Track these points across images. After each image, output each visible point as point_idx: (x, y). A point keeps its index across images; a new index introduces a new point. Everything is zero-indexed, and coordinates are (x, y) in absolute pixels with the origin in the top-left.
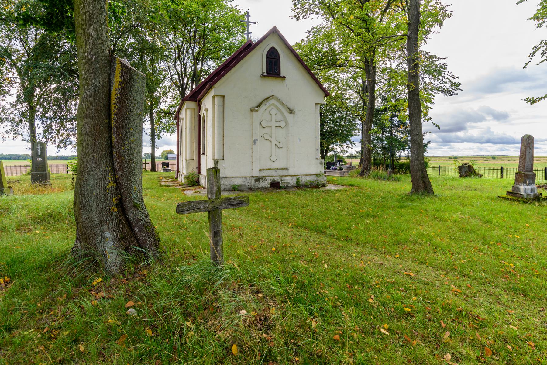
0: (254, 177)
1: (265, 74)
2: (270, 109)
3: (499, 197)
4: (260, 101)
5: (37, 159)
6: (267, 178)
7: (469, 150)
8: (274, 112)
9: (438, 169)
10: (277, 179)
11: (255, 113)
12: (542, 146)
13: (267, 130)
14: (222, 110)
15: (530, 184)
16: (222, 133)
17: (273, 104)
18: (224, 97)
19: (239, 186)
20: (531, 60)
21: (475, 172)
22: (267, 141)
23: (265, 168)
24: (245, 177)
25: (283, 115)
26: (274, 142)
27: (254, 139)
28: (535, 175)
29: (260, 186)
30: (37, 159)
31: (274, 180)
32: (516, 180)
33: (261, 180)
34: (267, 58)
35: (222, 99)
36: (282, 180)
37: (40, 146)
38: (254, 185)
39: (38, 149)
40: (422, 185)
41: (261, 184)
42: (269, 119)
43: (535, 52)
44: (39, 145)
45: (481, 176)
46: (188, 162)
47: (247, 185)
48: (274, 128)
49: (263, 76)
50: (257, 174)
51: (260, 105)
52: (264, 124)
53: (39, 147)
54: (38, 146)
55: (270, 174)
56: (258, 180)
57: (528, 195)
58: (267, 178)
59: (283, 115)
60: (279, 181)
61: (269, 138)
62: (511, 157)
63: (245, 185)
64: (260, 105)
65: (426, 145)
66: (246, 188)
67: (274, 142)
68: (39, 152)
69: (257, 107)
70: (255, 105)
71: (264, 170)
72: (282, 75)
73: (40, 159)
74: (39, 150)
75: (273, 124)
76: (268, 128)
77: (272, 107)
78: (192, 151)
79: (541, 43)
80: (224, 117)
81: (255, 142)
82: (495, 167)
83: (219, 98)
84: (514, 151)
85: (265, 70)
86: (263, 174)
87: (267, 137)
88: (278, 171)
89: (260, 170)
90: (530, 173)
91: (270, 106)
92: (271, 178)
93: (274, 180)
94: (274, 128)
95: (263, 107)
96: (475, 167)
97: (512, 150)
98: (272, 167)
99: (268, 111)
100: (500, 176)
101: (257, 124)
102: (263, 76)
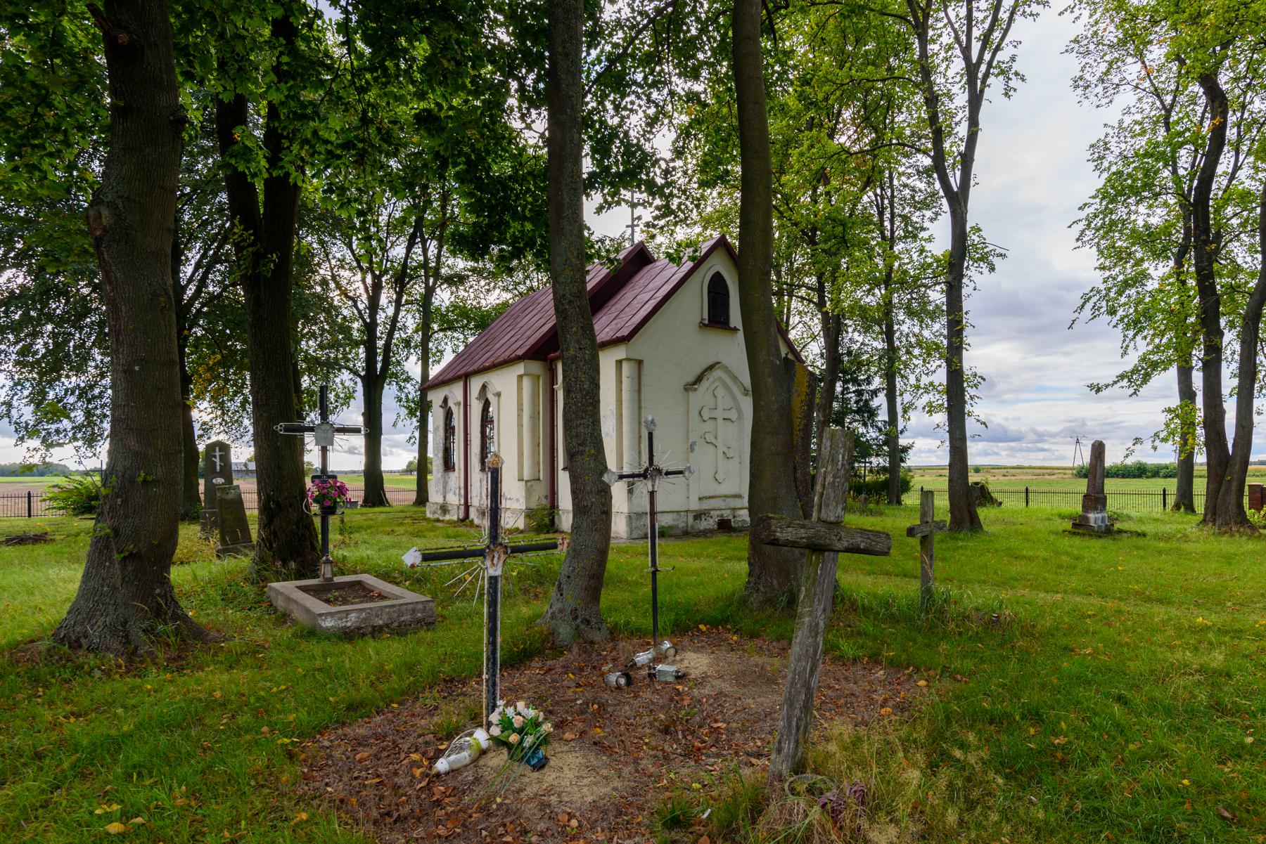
0: (692, 511)
1: (706, 322)
2: (714, 386)
3: (1065, 531)
4: (699, 371)
5: (214, 481)
6: (712, 513)
7: (928, 455)
8: (720, 392)
9: (1024, 495)
10: (727, 514)
11: (692, 395)
12: (1053, 447)
13: (709, 426)
14: (636, 388)
15: (1101, 511)
16: (637, 430)
17: (720, 379)
18: (640, 363)
19: (671, 527)
20: (1080, 316)
21: (991, 498)
22: (710, 446)
23: (707, 494)
24: (677, 512)
25: (734, 398)
26: (721, 448)
27: (691, 441)
28: (1105, 498)
29: (702, 528)
30: (214, 481)
31: (722, 516)
32: (1084, 507)
33: (703, 517)
34: (709, 292)
35: (636, 367)
36: (734, 517)
37: (220, 451)
38: (692, 527)
39: (215, 457)
40: (968, 519)
41: (704, 524)
42: (713, 406)
43: (1085, 303)
44: (217, 449)
45: (1001, 503)
46: (529, 484)
47: (681, 526)
48: (720, 421)
49: (703, 326)
50: (695, 505)
51: (699, 380)
52: (706, 415)
53: (218, 454)
54: (215, 451)
55: (716, 506)
56: (698, 516)
57: (1100, 527)
58: (712, 513)
59: (734, 398)
60: (731, 517)
61: (714, 441)
62: (1005, 468)
63: (677, 527)
64: (699, 380)
65: (905, 449)
66: (679, 532)
67: (721, 448)
68: (218, 463)
69: (695, 383)
70: (691, 379)
71: (707, 498)
72: (732, 325)
73: (220, 480)
74: (217, 460)
75: (720, 414)
76: (711, 423)
77: (717, 383)
78: (536, 464)
79: (1092, 291)
80: (640, 401)
81: (692, 448)
82: (1017, 489)
83: (632, 363)
84: (1008, 456)
85: (706, 316)
86: (706, 505)
87: (710, 438)
88: (728, 500)
89: (700, 499)
90: (1101, 496)
91: (714, 382)
92: (718, 512)
93: (722, 516)
94: (720, 421)
95: (705, 384)
96: (991, 488)
97: (1004, 453)
98: (717, 494)
99: (710, 392)
100: (1024, 504)
101: (694, 414)
102: (703, 326)
